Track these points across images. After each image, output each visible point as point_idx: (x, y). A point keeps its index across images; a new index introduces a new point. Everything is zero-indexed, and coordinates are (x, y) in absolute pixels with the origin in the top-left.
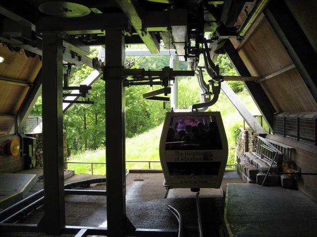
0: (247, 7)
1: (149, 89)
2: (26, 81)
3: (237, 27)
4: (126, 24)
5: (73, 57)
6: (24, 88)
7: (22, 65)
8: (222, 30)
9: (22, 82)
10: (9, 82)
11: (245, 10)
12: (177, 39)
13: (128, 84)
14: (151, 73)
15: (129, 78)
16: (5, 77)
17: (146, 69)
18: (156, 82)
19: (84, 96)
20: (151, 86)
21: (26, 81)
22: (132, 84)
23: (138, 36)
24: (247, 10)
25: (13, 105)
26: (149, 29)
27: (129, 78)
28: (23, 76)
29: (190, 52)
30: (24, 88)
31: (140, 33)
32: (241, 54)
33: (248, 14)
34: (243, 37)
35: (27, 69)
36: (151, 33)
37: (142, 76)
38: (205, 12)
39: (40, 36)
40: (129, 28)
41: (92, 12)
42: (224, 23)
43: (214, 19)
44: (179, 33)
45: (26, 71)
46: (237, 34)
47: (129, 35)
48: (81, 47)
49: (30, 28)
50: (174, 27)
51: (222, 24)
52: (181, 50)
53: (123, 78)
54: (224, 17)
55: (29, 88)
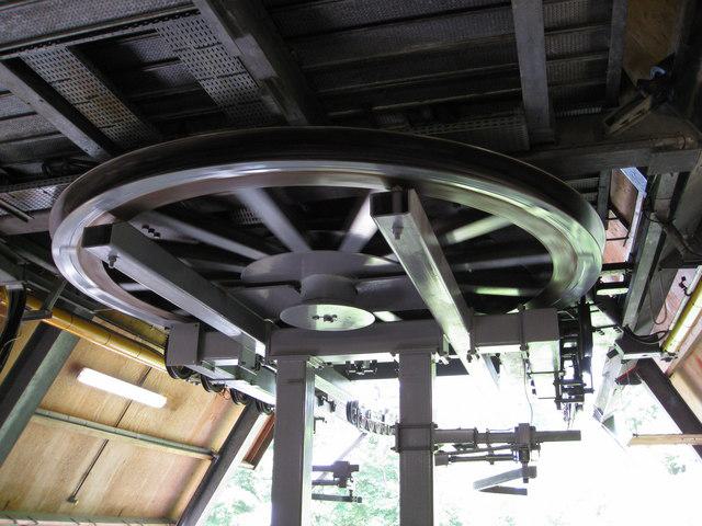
0: (684, 279)
1: (486, 470)
2: (204, 448)
3: (660, 335)
4: (434, 336)
5: (321, 403)
6: (199, 461)
7: (201, 414)
8: (629, 341)
9: (197, 449)
10: (171, 450)
11: (682, 285)
12: (536, 366)
13: (445, 459)
14: (489, 437)
15: (448, 447)
16: (159, 437)
17: (482, 430)
18: (259, 439)
19: (342, 484)
20: (492, 463)
21: (204, 448)
22: (454, 459)
23: (458, 361)
24: (685, 283)
25: (175, 501)
26: (482, 350)
27: (448, 447)
28: (200, 437)
29: (564, 390)
30: (199, 461)
31: (462, 355)
32: (677, 382)
33: (689, 292)
34: (673, 354)
35: (210, 422)
36: (484, 355)
37: (469, 442)
38: (592, 309)
39: (273, 365)
40: (446, 348)
41: (378, 320)
42: (632, 328)
43: (610, 321)
44: (545, 353)
45: (207, 426)
46: (661, 350)
47: (446, 362)
48: (336, 383)
49: (268, 351)
50: (532, 345)
51: (627, 330)
52: (546, 386)
53: (436, 448)
54: (630, 317)
55: (209, 462)
